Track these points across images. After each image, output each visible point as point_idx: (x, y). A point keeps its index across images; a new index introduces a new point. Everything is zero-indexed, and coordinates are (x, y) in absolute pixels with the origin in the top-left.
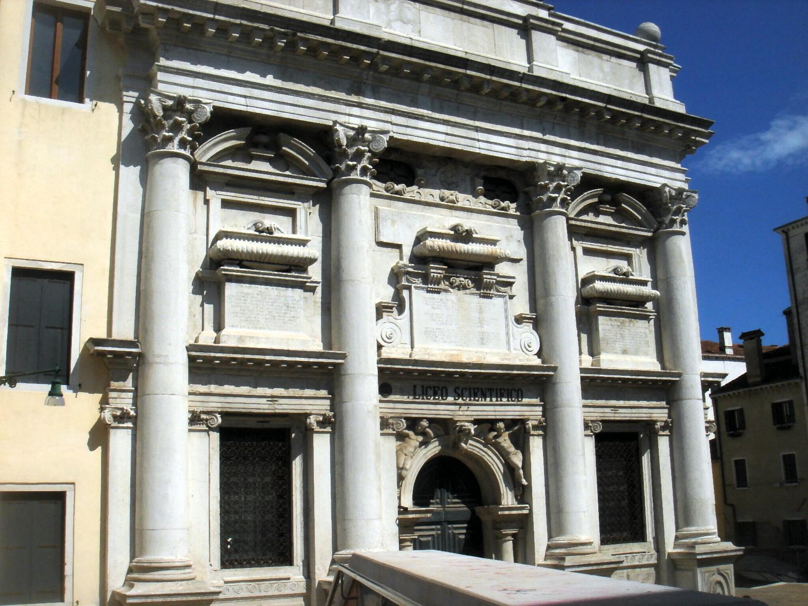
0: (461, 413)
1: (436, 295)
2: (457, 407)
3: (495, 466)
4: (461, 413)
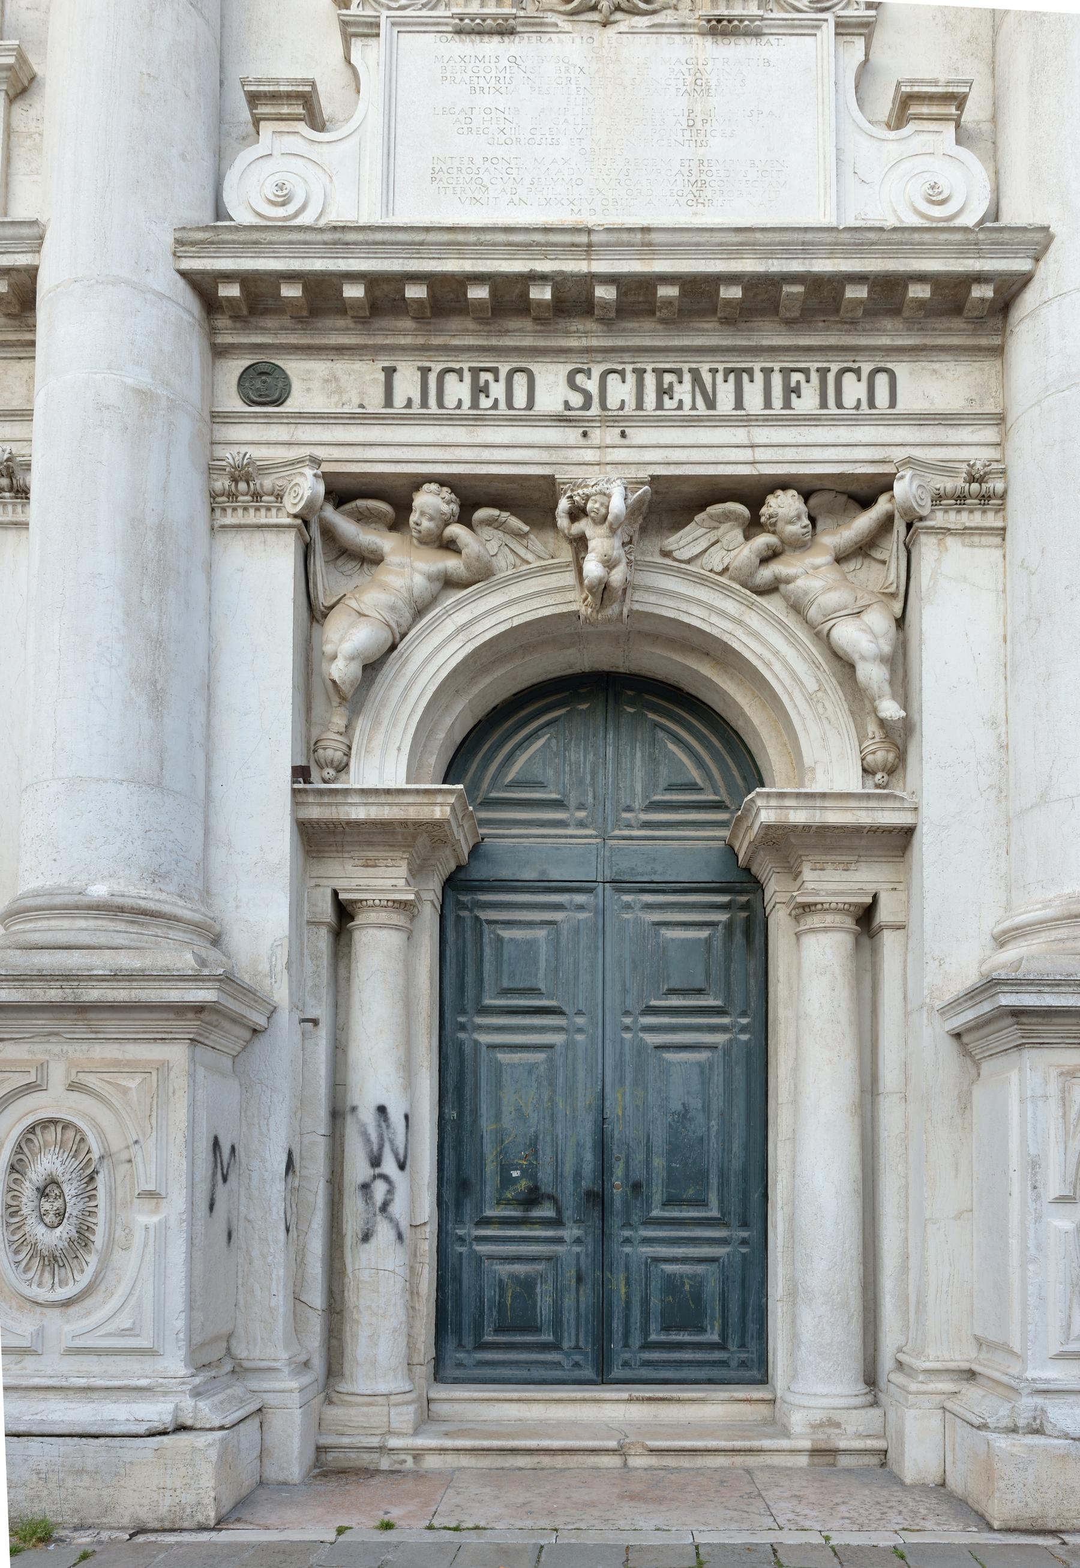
0: (589, 455)
1: (492, 46)
2: (572, 435)
3: (777, 667)
4: (589, 455)
